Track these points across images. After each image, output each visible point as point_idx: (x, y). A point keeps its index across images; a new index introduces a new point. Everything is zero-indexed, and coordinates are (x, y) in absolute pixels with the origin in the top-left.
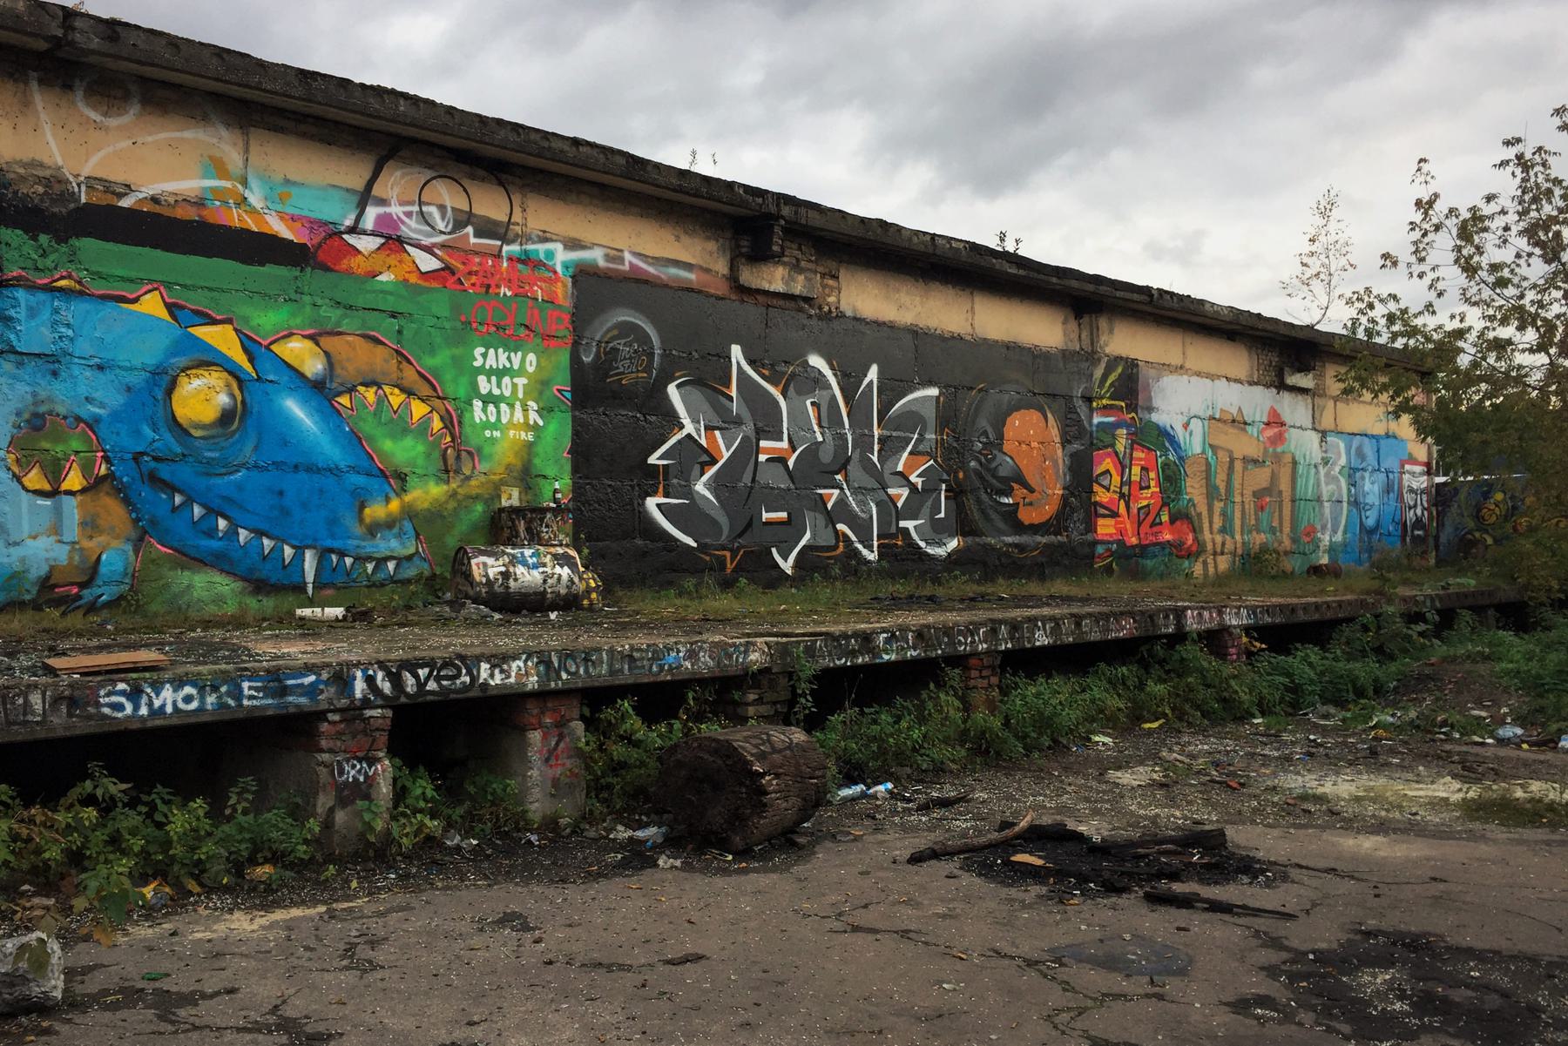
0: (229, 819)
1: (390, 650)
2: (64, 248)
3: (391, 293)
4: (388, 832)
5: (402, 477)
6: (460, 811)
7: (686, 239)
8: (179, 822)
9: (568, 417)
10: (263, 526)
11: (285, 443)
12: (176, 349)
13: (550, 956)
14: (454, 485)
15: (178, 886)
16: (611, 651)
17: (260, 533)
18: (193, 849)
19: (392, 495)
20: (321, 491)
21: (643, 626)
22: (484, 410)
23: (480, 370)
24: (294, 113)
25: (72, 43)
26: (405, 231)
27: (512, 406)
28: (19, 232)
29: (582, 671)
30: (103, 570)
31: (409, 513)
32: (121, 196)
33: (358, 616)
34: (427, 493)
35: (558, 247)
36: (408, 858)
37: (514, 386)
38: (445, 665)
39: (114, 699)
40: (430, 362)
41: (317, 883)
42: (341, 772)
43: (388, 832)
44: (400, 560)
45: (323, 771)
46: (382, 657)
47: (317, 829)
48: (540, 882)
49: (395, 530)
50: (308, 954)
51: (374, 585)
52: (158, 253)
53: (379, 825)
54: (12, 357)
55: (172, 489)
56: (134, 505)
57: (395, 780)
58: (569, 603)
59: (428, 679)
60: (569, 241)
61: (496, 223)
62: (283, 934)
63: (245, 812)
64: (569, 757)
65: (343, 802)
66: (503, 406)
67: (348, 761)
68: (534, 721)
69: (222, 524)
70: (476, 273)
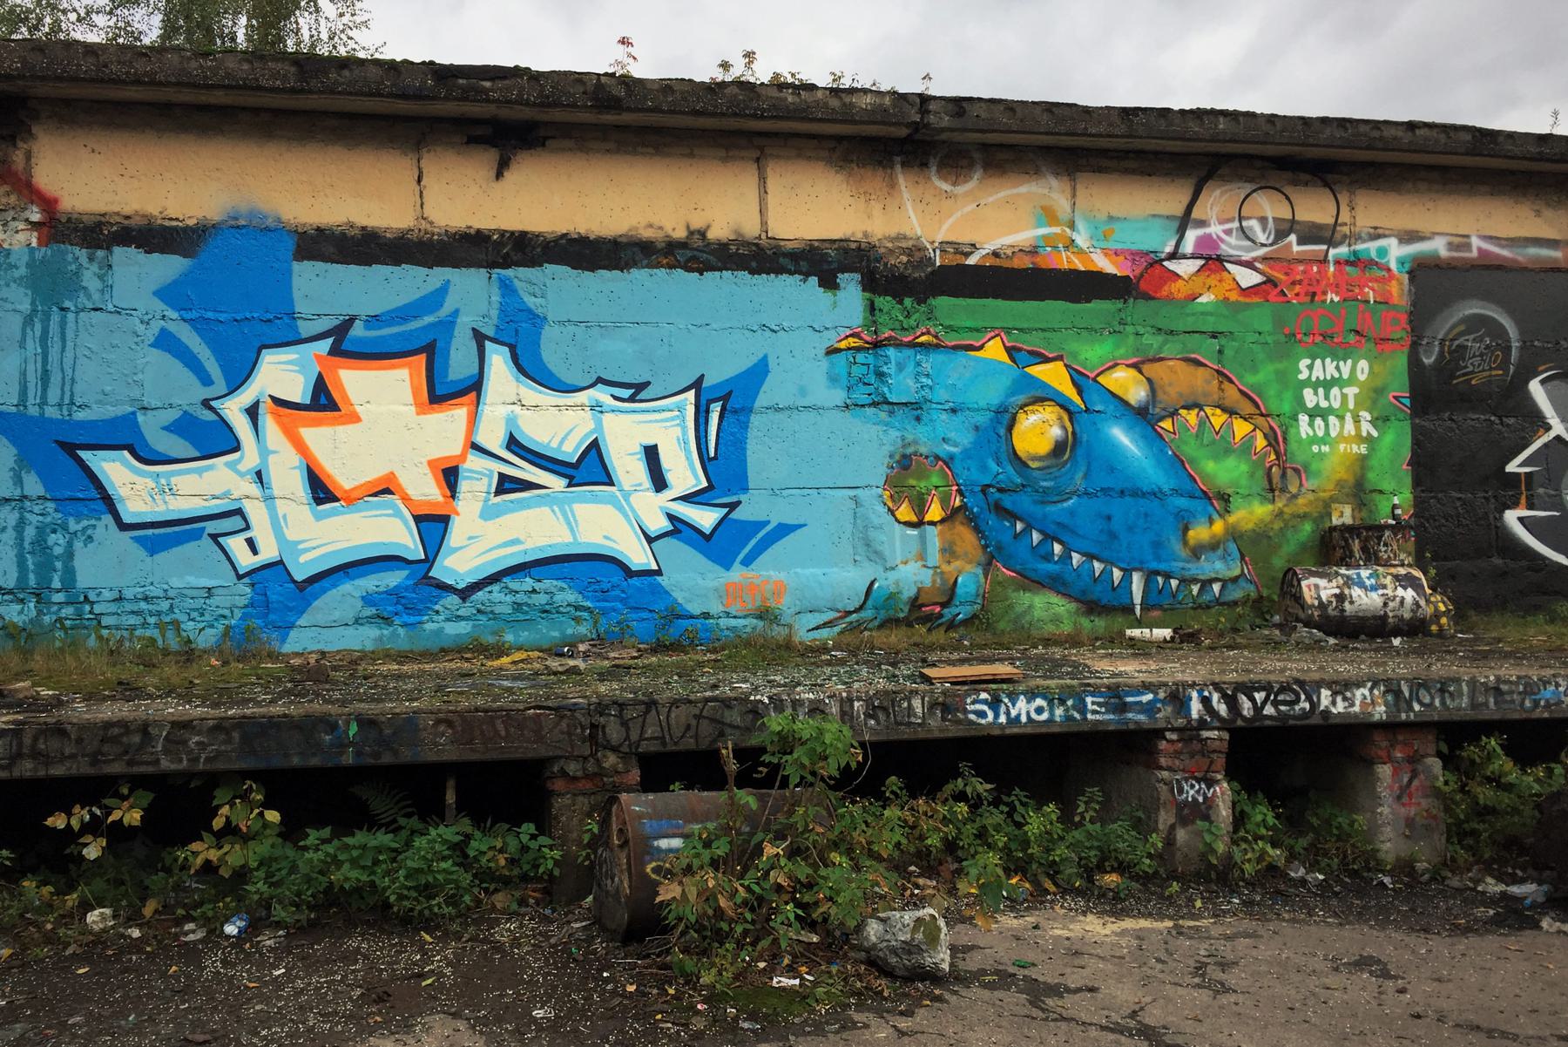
0: (1080, 824)
1: (1223, 672)
2: (923, 308)
3: (1211, 314)
4: (1229, 856)
5: (1225, 498)
6: (1303, 842)
7: (1548, 213)
8: (1035, 824)
9: (1406, 427)
10: (1094, 551)
11: (1112, 470)
12: (1013, 391)
13: (1418, 1009)
14: (1280, 504)
15: (1036, 883)
16: (1473, 682)
17: (1091, 557)
18: (1048, 851)
19: (1215, 516)
20: (1146, 515)
21: (1506, 656)
22: (1311, 425)
23: (1307, 383)
24: (1115, 151)
25: (927, 126)
26: (1225, 249)
27: (1341, 418)
28: (889, 298)
29: (1437, 702)
30: (959, 591)
31: (1234, 535)
32: (967, 255)
33: (1185, 638)
34: (1251, 513)
35: (1392, 243)
36: (1250, 884)
37: (1344, 397)
38: (1283, 689)
39: (979, 707)
40: (1251, 379)
41: (1161, 897)
42: (1181, 791)
43: (1229, 856)
44: (1225, 583)
45: (1163, 788)
46: (1217, 679)
47: (1160, 845)
48: (1398, 928)
49: (1220, 552)
50: (1159, 966)
51: (1200, 607)
52: (1000, 302)
53: (1221, 847)
54: (886, 407)
55: (1014, 516)
56: (982, 532)
57: (1234, 804)
58: (1415, 628)
59: (1265, 702)
60: (1398, 234)
61: (1320, 227)
62: (1135, 943)
63: (1092, 821)
64: (1427, 796)
65: (1184, 821)
66: (1332, 419)
67: (1186, 780)
68: (1383, 754)
69: (1057, 548)
70: (1300, 282)
